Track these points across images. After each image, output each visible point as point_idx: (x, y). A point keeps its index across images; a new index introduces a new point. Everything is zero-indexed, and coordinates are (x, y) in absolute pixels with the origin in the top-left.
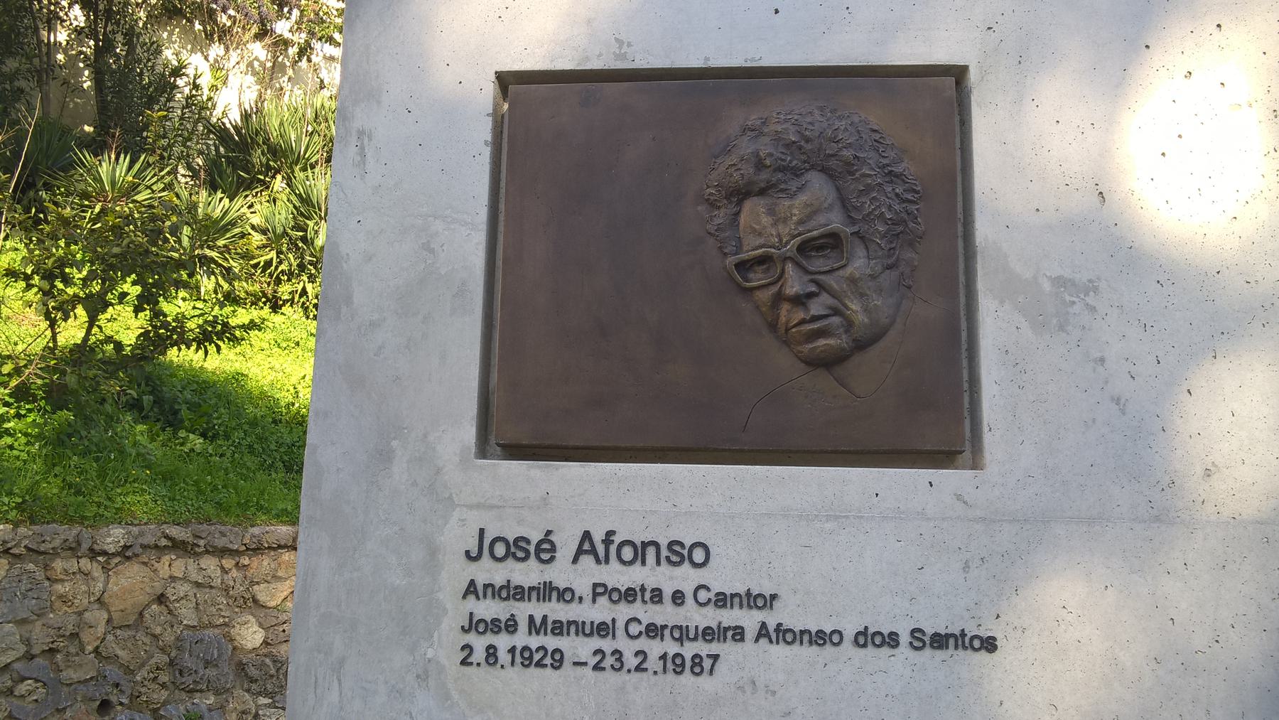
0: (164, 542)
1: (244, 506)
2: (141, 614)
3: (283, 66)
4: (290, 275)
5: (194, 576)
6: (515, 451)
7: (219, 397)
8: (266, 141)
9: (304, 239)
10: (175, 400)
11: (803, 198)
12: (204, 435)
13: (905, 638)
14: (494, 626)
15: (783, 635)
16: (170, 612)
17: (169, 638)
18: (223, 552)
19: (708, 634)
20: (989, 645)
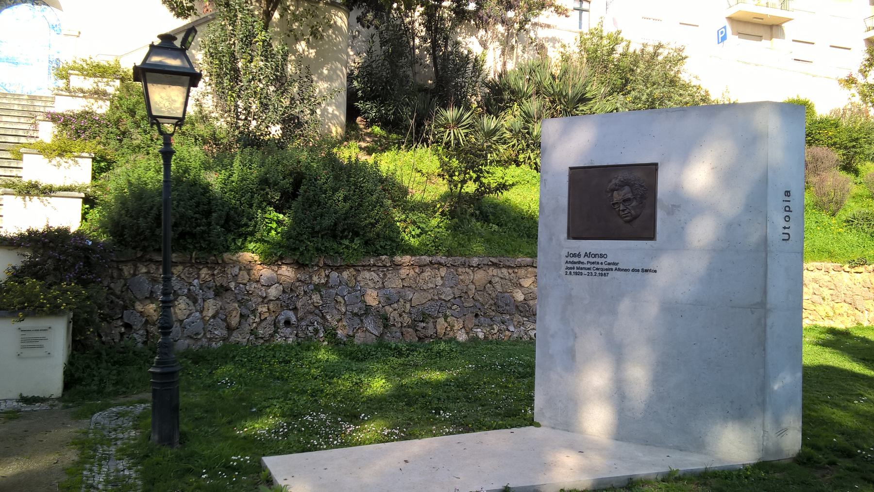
0: (490, 263)
1: (514, 251)
2: (485, 287)
3: (512, 33)
4: (523, 150)
5: (500, 275)
6: (575, 238)
7: (502, 210)
8: (509, 88)
9: (528, 133)
10: (487, 212)
11: (623, 192)
12: (497, 225)
13: (640, 270)
14: (571, 268)
15: (619, 270)
16: (493, 287)
17: (494, 295)
18: (509, 267)
19: (607, 270)
20: (655, 271)
